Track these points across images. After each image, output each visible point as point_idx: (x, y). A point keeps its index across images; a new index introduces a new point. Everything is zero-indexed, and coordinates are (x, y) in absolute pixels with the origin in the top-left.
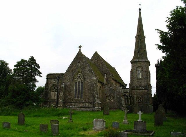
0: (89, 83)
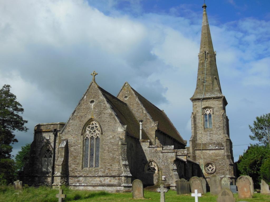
0: (111, 138)
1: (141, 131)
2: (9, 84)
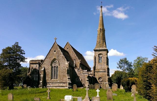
0: (63, 67)
1: (74, 64)
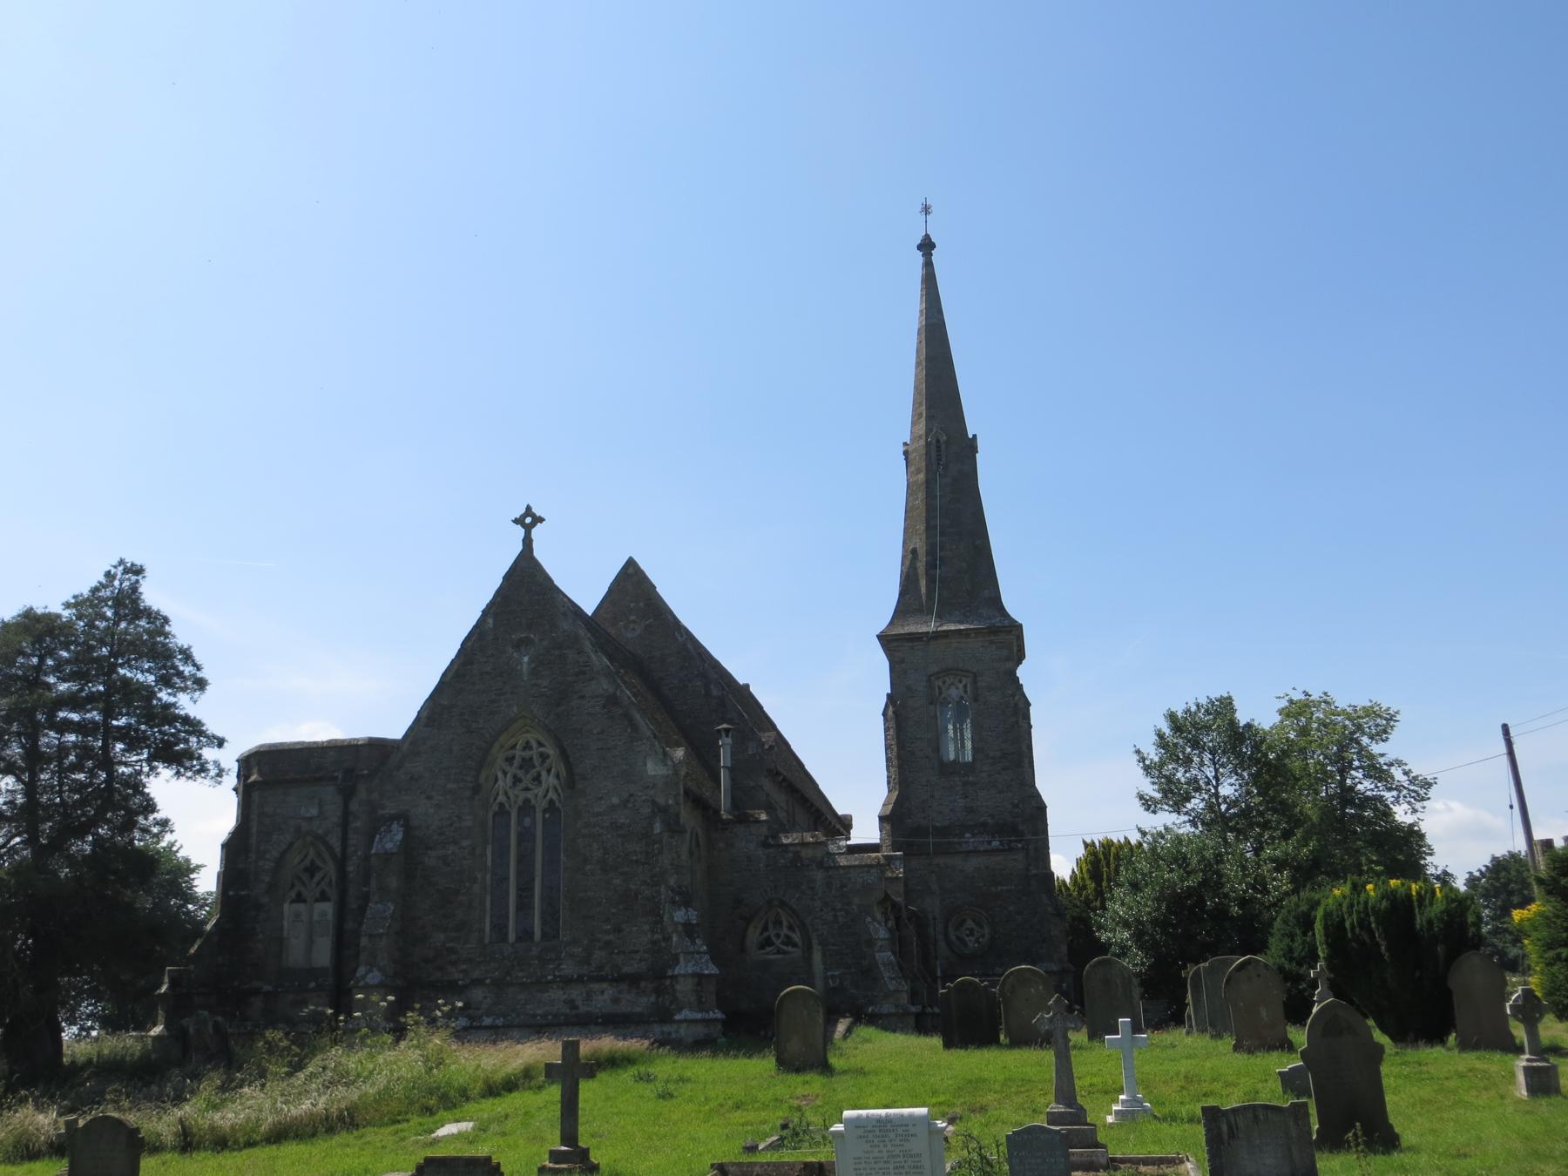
2: (138, 562)
